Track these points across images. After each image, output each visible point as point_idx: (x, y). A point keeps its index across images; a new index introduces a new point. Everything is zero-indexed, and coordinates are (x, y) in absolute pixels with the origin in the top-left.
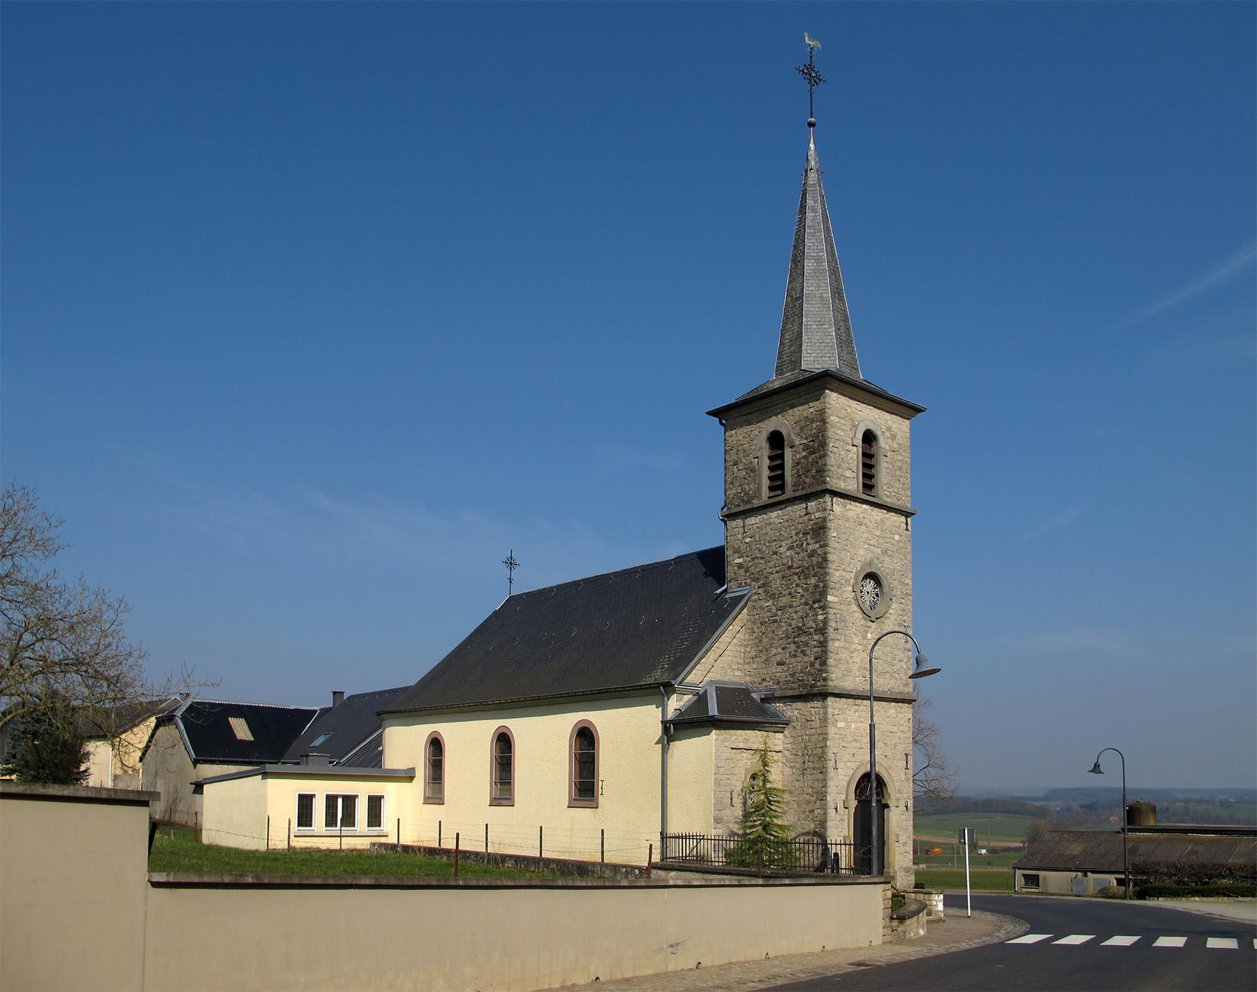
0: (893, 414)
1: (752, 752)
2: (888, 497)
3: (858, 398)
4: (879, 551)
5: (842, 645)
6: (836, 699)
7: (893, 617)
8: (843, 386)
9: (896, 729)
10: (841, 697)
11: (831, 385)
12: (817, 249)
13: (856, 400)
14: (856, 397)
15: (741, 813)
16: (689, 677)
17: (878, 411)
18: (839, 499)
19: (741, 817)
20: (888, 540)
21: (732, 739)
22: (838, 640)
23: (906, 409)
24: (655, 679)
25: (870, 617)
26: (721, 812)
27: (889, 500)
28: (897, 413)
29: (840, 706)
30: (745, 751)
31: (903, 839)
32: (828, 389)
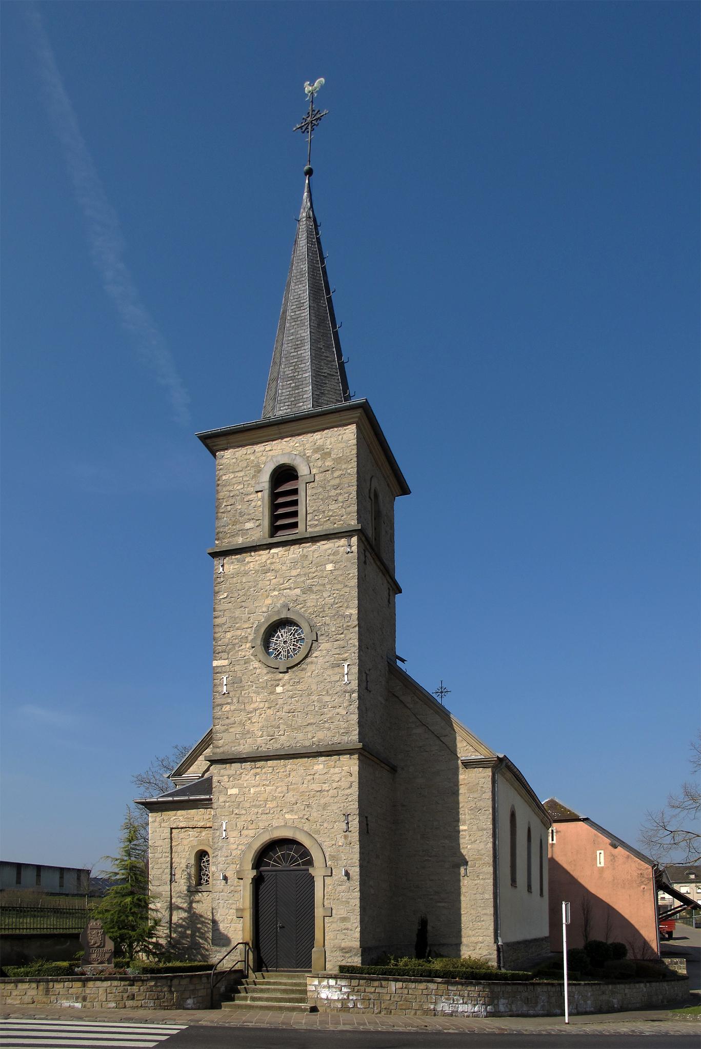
0: (323, 430)
1: (199, 830)
2: (316, 526)
3: (244, 443)
4: (298, 591)
5: (233, 708)
6: (225, 766)
7: (321, 660)
8: (232, 438)
9: (326, 787)
10: (231, 763)
11: (218, 445)
12: (295, 315)
13: (263, 442)
14: (263, 439)
15: (185, 888)
16: (191, 768)
17: (300, 437)
18: (233, 557)
19: (186, 892)
20: (315, 575)
21: (172, 819)
22: (228, 703)
23: (337, 415)
24: (285, 766)
25: (278, 668)
26: (160, 887)
27: (317, 529)
28: (328, 425)
29: (232, 772)
30: (191, 830)
31: (340, 911)
32: (218, 451)
